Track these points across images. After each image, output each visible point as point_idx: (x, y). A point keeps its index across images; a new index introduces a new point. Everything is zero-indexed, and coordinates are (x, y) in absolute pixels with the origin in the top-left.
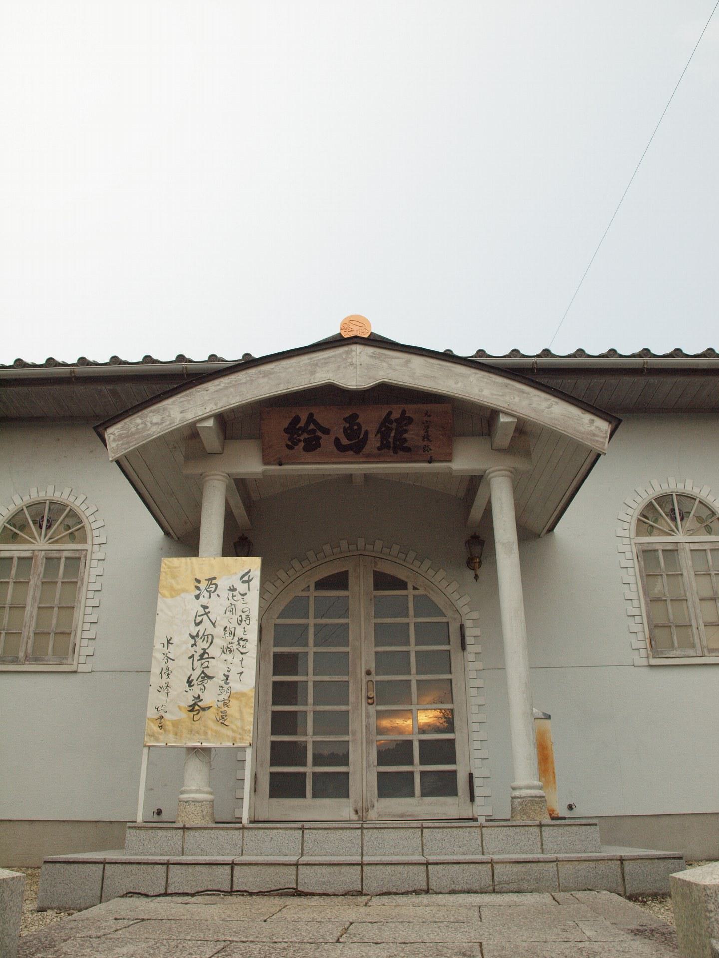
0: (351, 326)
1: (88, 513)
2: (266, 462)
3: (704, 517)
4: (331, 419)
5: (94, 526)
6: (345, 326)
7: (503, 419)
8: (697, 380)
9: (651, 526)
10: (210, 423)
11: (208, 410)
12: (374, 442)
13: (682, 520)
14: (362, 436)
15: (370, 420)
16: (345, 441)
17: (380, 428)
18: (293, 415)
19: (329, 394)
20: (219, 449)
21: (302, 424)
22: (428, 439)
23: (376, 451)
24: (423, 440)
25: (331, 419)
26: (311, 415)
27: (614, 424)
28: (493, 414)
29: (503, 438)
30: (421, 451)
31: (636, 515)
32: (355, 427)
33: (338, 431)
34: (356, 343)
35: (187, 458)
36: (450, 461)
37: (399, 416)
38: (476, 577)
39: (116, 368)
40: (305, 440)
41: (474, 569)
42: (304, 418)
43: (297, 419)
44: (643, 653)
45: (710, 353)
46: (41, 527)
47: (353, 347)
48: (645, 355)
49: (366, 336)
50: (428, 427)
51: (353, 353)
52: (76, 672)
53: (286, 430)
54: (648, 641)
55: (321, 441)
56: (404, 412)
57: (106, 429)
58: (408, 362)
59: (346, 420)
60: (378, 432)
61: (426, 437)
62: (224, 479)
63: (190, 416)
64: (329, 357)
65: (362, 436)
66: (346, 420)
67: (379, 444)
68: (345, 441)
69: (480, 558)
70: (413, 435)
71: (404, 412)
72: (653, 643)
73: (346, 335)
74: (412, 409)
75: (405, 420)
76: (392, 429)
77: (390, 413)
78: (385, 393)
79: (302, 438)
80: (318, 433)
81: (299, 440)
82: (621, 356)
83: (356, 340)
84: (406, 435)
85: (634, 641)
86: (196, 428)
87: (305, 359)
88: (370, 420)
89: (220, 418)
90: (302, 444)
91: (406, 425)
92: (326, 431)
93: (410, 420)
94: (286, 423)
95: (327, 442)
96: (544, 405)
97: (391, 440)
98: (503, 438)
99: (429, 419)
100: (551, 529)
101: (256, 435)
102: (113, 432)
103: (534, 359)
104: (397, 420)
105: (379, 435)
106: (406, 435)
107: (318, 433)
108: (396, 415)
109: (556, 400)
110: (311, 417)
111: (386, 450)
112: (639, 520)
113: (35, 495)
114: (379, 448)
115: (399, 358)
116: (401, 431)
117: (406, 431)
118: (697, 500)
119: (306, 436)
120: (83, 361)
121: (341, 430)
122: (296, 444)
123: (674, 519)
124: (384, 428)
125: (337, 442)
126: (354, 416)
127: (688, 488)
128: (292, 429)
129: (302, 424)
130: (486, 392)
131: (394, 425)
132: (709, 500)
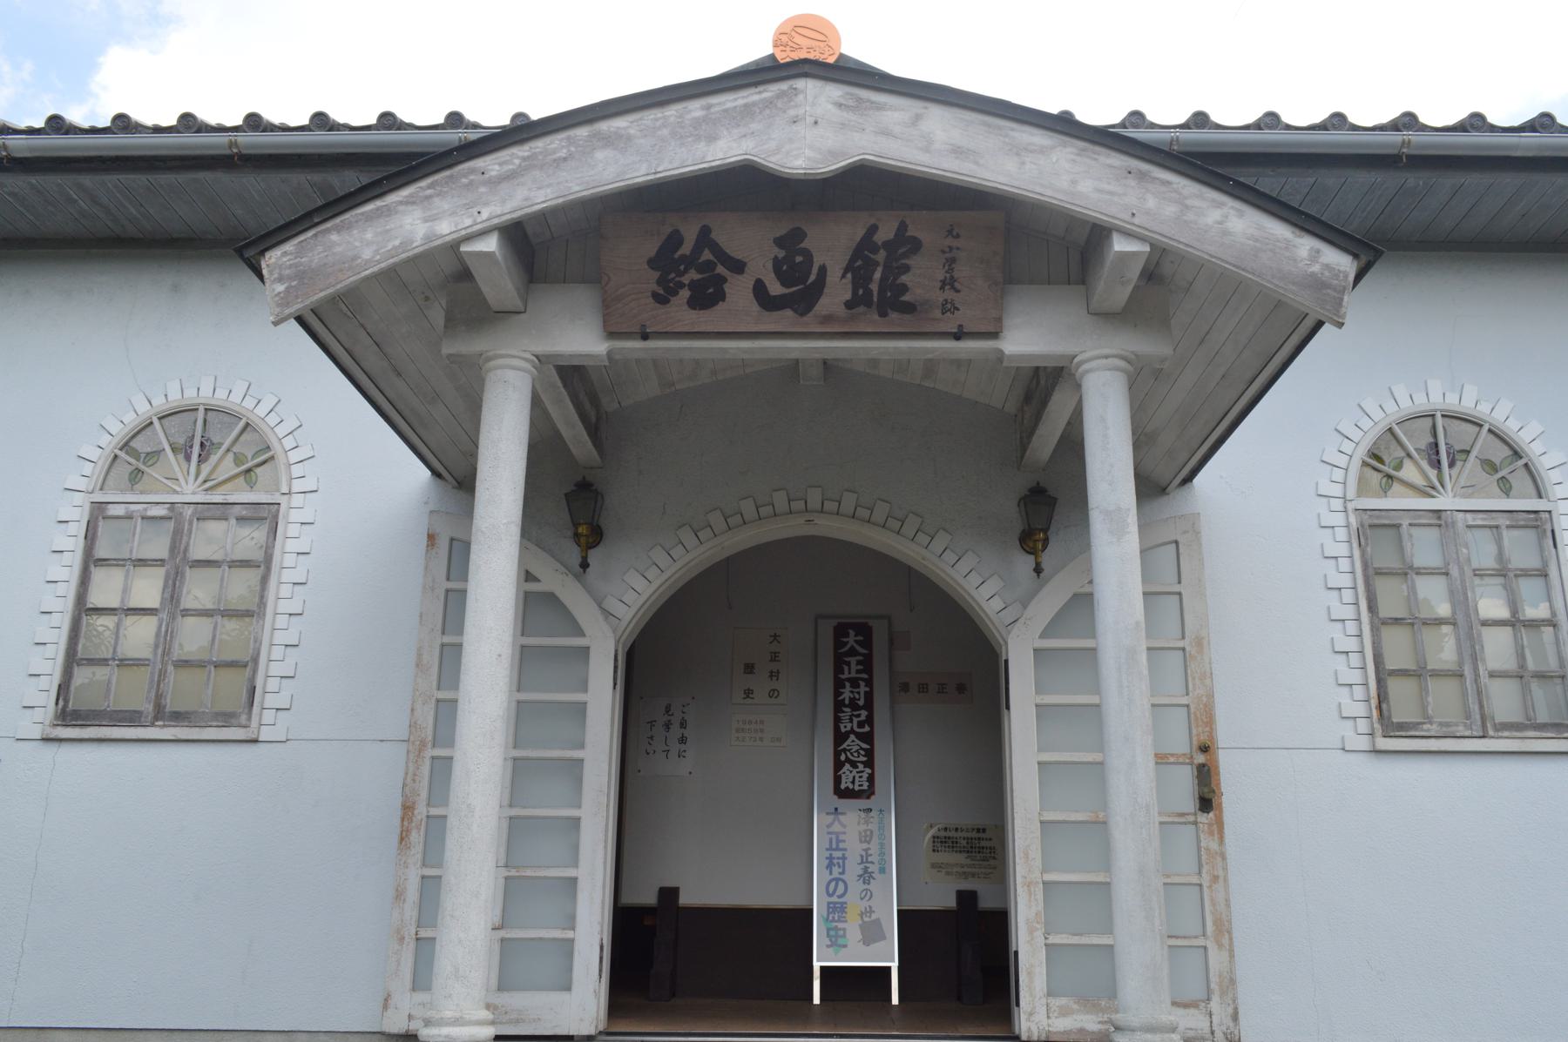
0: (798, 39)
1: (281, 431)
2: (612, 335)
3: (1497, 461)
4: (752, 243)
5: (294, 456)
6: (784, 38)
7: (1120, 245)
8: (1509, 181)
9: (1389, 477)
10: (491, 244)
11: (485, 215)
12: (837, 293)
13: (1452, 465)
14: (812, 278)
15: (831, 246)
16: (775, 288)
17: (852, 261)
18: (668, 230)
19: (746, 186)
20: (519, 305)
21: (686, 249)
22: (953, 288)
23: (841, 311)
24: (942, 288)
25: (752, 243)
26: (705, 232)
27: (1364, 259)
28: (1097, 234)
29: (1114, 289)
30: (937, 313)
31: (1361, 453)
32: (799, 259)
33: (761, 263)
34: (806, 75)
35: (451, 322)
36: (995, 335)
37: (891, 236)
38: (1038, 570)
39: (321, 137)
40: (693, 286)
41: (1032, 552)
42: (690, 235)
43: (675, 240)
44: (1363, 725)
45: (1544, 122)
46: (188, 458)
47: (800, 83)
48: (1408, 127)
49: (831, 60)
50: (952, 261)
51: (801, 97)
52: (255, 741)
53: (652, 263)
54: (1374, 702)
55: (726, 287)
56: (903, 227)
57: (262, 253)
58: (918, 117)
59: (779, 242)
60: (846, 271)
61: (949, 283)
62: (528, 366)
63: (446, 228)
64: (1212, 900)
65: (812, 278)
66: (779, 242)
67: (848, 296)
68: (775, 288)
69: (1046, 531)
70: (921, 279)
71: (903, 227)
72: (1384, 706)
73: (783, 57)
74: (922, 227)
75: (904, 244)
76: (877, 264)
77: (873, 229)
78: (865, 186)
79: (686, 280)
80: (720, 269)
81: (682, 286)
82: (1355, 128)
83: (807, 68)
84: (904, 279)
85: (1345, 700)
86: (459, 257)
87: (695, 108)
88: (831, 246)
89: (517, 234)
90: (685, 294)
91: (905, 255)
92: (738, 267)
93: (916, 246)
94: (651, 248)
95: (739, 291)
96: (1213, 216)
97: (874, 287)
98: (1114, 289)
99: (955, 243)
100: (1189, 479)
101: (591, 275)
102: (273, 259)
103: (1173, 134)
104: (886, 245)
105: (849, 275)
106: (904, 279)
107: (720, 269)
108: (885, 233)
109: (1238, 204)
110: (705, 236)
111: (862, 309)
112: (1365, 464)
113: (1439, 396)
114: (849, 305)
115: (898, 111)
116: (896, 268)
117: (907, 269)
118: (1486, 427)
119: (693, 275)
120: (254, 122)
121: (770, 265)
122: (675, 293)
123: (1437, 464)
124: (858, 266)
125: (759, 289)
126: (797, 235)
127: (1468, 400)
128: (667, 262)
129: (686, 249)
130: (1086, 187)
131: (881, 256)
132: (1511, 427)
